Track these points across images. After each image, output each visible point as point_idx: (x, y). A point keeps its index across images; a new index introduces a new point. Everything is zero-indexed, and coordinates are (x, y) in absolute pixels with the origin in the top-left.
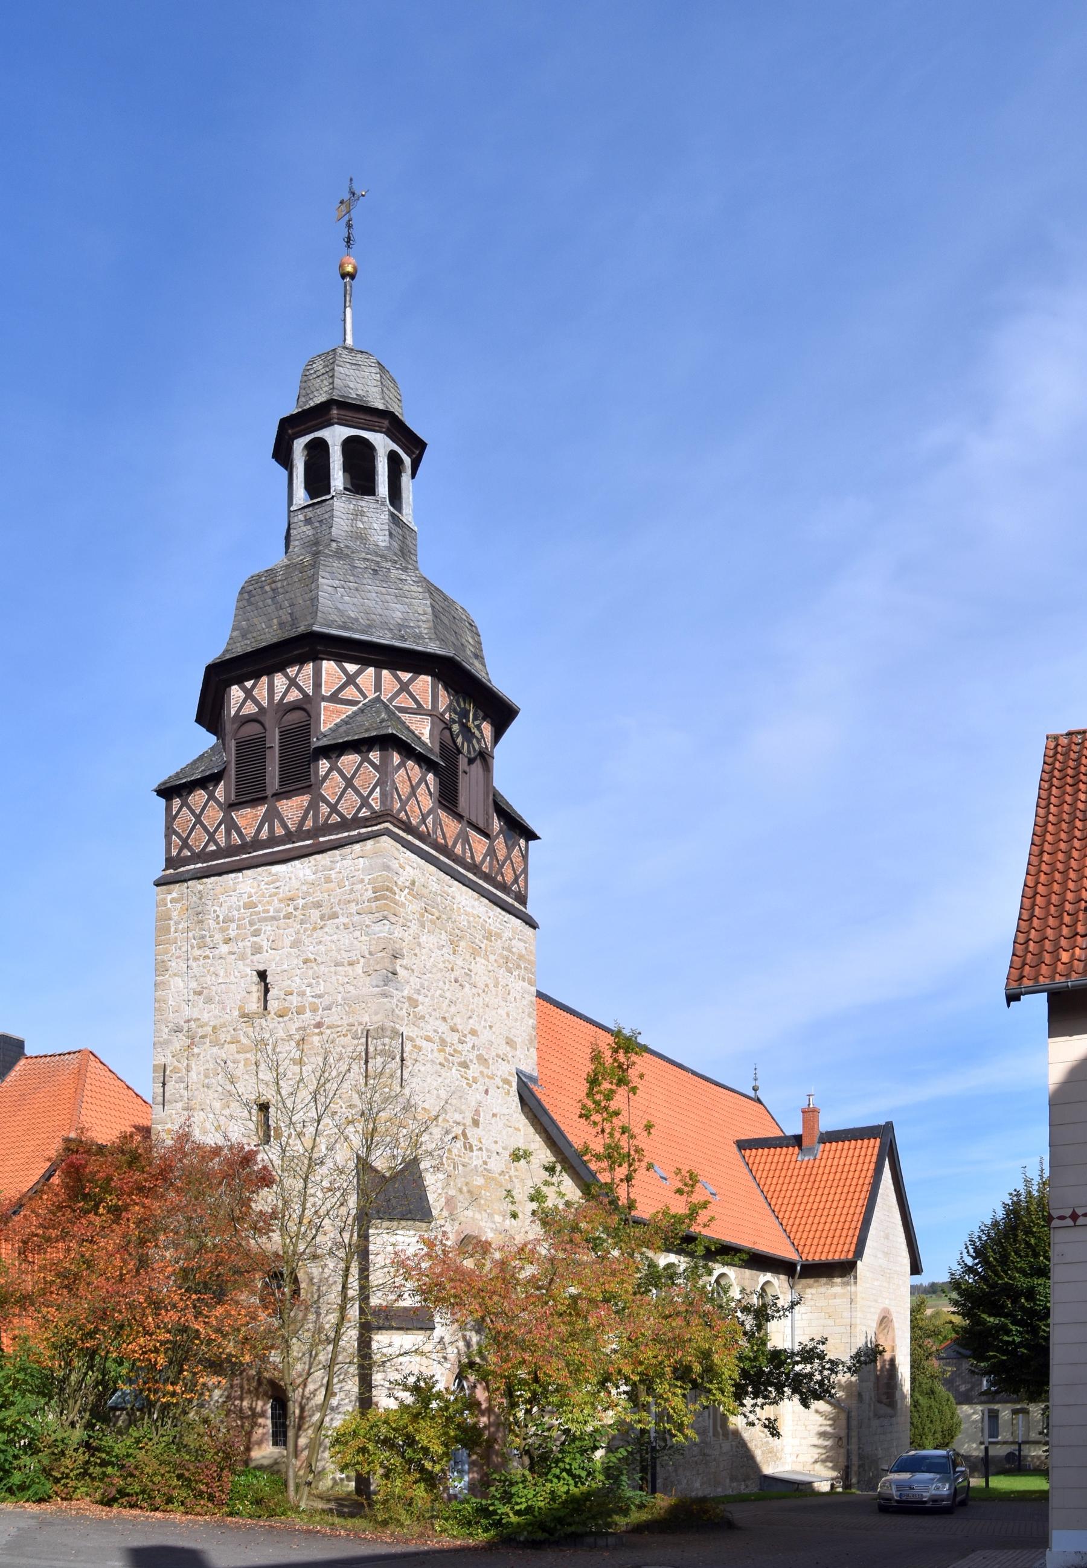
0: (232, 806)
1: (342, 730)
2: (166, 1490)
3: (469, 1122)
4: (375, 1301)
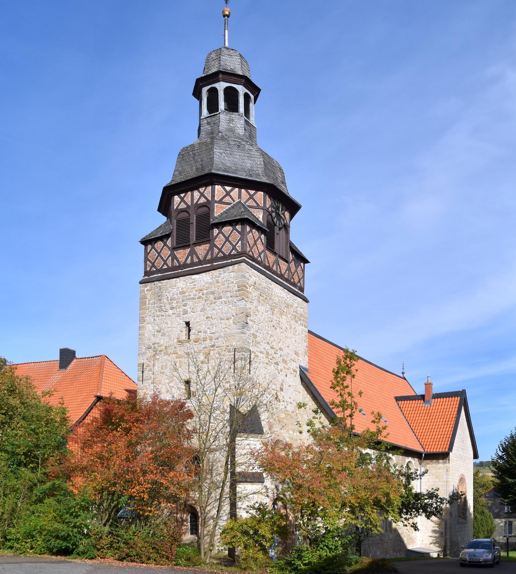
0: (174, 249)
1: (224, 216)
2: (147, 554)
3: (278, 389)
4: (238, 470)
